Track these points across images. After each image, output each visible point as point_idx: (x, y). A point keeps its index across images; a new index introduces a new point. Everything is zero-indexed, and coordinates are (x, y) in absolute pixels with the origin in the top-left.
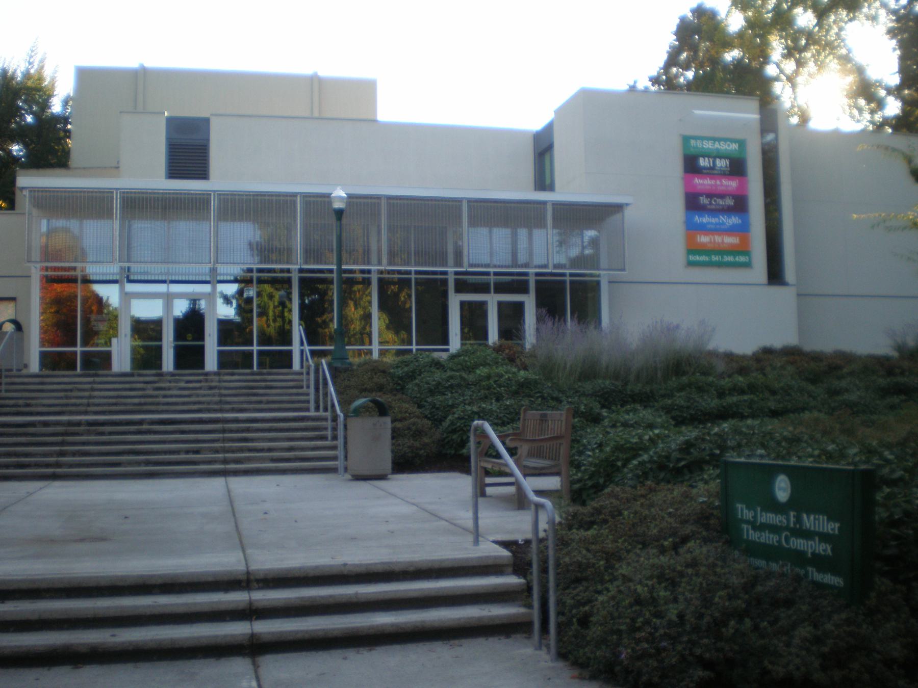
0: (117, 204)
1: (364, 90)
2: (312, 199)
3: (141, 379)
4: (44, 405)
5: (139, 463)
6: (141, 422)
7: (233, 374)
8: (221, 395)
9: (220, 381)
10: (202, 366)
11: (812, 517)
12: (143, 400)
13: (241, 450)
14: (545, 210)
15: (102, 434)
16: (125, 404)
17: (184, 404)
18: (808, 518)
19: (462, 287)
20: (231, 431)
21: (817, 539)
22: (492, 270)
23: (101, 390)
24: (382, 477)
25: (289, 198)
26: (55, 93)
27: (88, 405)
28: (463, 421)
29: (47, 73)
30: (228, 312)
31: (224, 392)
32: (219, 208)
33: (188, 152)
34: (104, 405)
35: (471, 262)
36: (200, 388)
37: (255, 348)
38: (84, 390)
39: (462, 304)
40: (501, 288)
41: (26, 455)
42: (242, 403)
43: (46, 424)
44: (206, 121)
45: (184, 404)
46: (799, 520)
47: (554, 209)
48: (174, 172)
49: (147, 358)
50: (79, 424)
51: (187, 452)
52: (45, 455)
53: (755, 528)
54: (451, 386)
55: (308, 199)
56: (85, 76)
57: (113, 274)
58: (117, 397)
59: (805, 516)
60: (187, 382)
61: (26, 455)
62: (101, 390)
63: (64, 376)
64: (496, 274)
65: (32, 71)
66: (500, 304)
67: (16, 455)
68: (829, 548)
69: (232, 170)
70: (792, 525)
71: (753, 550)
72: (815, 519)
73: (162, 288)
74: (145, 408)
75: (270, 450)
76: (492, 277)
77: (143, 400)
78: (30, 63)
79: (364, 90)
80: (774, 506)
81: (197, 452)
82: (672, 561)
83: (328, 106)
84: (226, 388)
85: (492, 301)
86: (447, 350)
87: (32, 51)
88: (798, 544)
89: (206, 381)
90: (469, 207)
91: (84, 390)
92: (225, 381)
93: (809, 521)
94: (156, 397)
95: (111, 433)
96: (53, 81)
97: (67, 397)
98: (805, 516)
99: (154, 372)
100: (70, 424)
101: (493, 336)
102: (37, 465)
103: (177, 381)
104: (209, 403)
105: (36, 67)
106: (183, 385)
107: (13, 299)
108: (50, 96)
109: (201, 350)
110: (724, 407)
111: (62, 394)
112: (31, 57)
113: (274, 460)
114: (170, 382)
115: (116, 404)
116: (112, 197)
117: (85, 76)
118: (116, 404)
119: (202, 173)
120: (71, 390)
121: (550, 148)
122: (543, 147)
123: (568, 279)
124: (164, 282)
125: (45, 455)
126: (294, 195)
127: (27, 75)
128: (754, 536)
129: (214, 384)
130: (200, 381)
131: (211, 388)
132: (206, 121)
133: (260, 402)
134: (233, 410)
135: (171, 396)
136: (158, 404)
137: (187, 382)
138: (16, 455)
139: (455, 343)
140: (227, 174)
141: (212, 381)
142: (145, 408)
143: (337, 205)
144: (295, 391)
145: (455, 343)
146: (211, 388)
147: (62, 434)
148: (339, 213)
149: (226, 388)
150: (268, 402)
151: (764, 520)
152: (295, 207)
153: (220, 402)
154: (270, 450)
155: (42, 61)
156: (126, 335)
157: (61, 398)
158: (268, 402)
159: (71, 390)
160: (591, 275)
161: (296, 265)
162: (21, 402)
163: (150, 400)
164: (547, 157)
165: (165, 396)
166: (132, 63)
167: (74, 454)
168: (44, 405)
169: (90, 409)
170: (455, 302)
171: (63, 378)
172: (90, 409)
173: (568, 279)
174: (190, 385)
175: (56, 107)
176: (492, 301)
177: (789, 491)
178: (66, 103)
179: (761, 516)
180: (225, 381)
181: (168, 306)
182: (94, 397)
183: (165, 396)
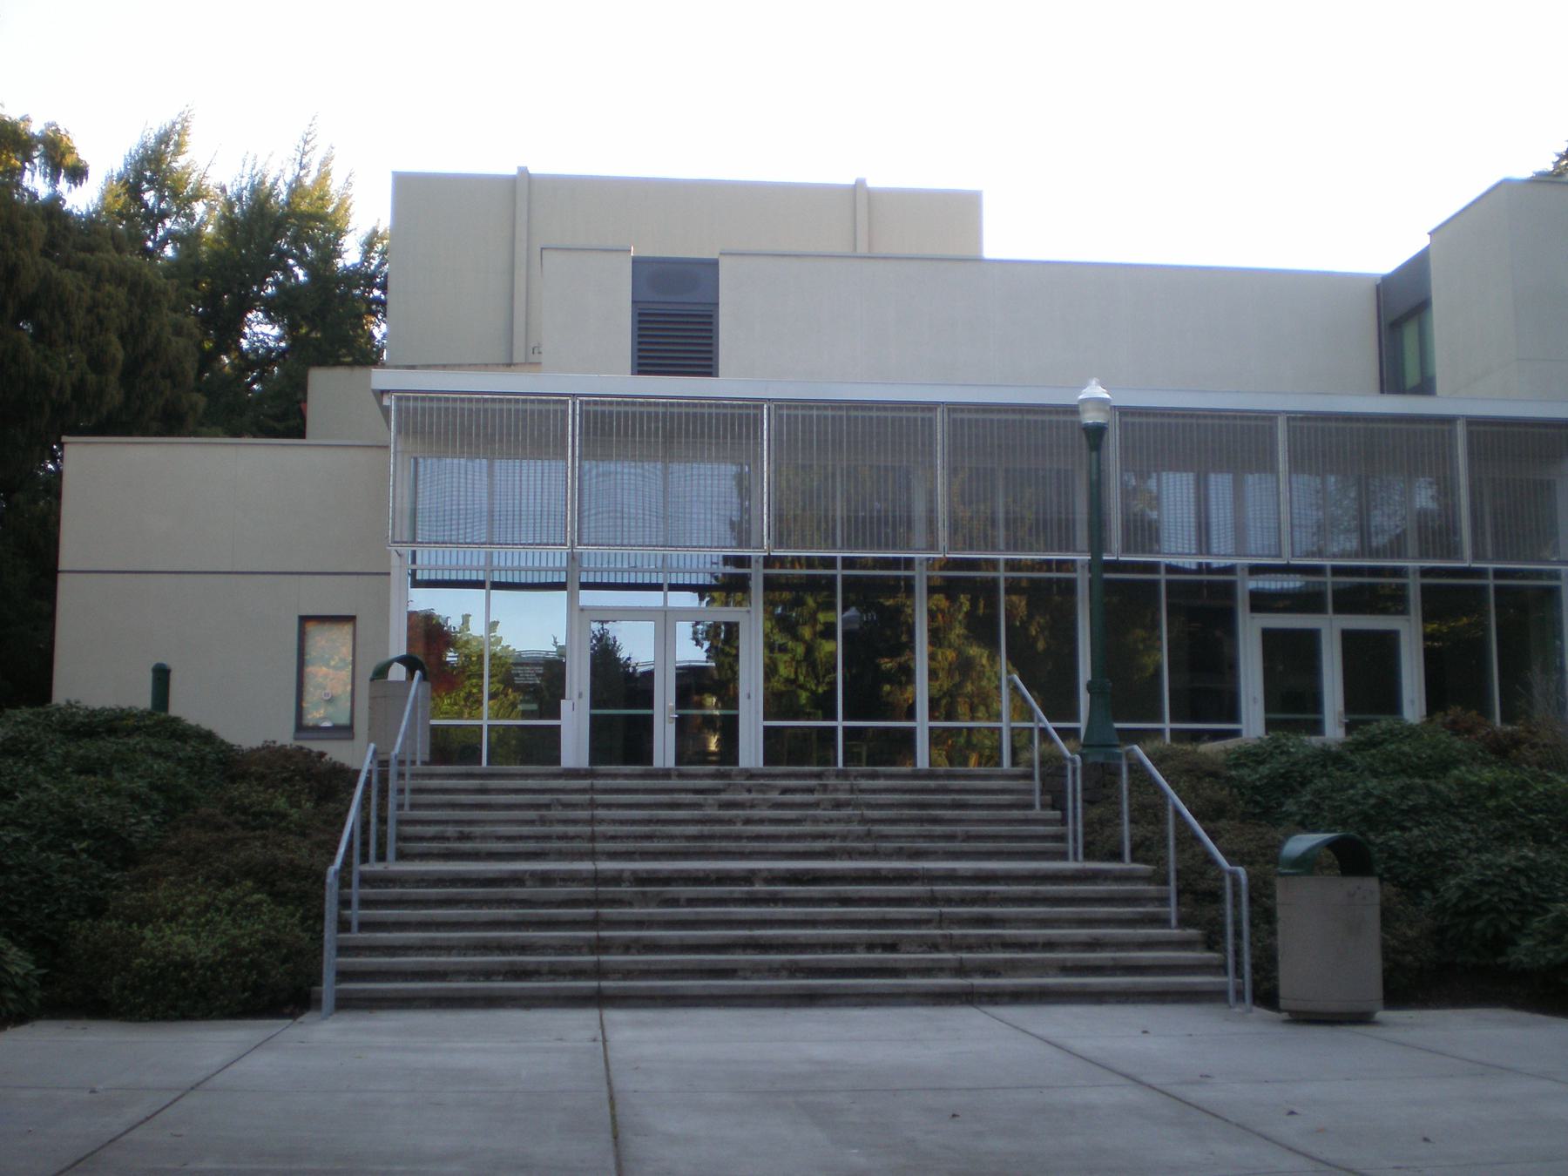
0: (573, 427)
1: (961, 209)
2: (966, 416)
3: (690, 783)
4: (499, 838)
5: (774, 971)
6: (748, 878)
7: (874, 776)
8: (863, 821)
9: (852, 791)
10: (648, 759)
12: (706, 829)
13: (987, 944)
14: (1452, 435)
15: (674, 902)
16: (671, 837)
17: (791, 837)
19: (1261, 602)
20: (949, 901)
22: (1328, 563)
23: (608, 806)
24: (1361, 1018)
25: (920, 415)
26: (351, 226)
27: (593, 838)
28: (1495, 889)
29: (335, 186)
30: (692, 653)
31: (869, 813)
32: (779, 433)
33: (676, 321)
34: (627, 837)
35: (347, 629)
36: (816, 805)
37: (840, 723)
38: (573, 806)
39: (1268, 635)
40: (1348, 602)
41: (523, 948)
42: (912, 837)
43: (545, 879)
44: (714, 264)
45: (791, 837)
47: (1470, 434)
48: (643, 365)
49: (622, 737)
50: (616, 879)
51: (871, 947)
52: (565, 948)
54: (1415, 810)
55: (959, 416)
56: (412, 191)
57: (554, 570)
58: (649, 822)
60: (785, 791)
61: (523, 948)
62: (608, 806)
63: (615, 776)
64: (1337, 571)
65: (308, 182)
66: (1348, 637)
67: (502, 948)
69: (757, 362)
73: (653, 599)
74: (716, 845)
75: (1050, 945)
76: (1329, 580)
77: (706, 829)
78: (302, 167)
79: (961, 209)
81: (892, 947)
83: (903, 240)
84: (870, 806)
85: (1330, 628)
86: (1235, 733)
87: (306, 142)
89: (825, 789)
90: (1291, 431)
91: (573, 806)
92: (862, 791)
94: (730, 822)
95: (691, 902)
96: (343, 206)
97: (543, 821)
99: (638, 768)
100: (597, 879)
101: (1413, 705)
102: (555, 972)
103: (763, 790)
104: (844, 838)
105: (314, 174)
106: (775, 796)
107: (351, 619)
108: (340, 233)
109: (645, 726)
111: (532, 814)
112: (304, 154)
113: (1066, 969)
114: (749, 791)
115: (649, 837)
116: (565, 413)
117: (412, 191)
118: (649, 837)
119: (706, 366)
120: (547, 806)
121: (1421, 308)
122: (1401, 310)
123: (1491, 582)
124: (657, 587)
125: (565, 948)
126: (931, 407)
127: (296, 188)
129: (843, 796)
130: (811, 790)
131: (838, 805)
132: (714, 264)
133: (951, 837)
134: (899, 854)
135: (761, 821)
136: (738, 838)
137: (785, 791)
138: (502, 948)
139: (1252, 722)
140: (751, 366)
141: (836, 790)
142: (716, 845)
143: (1091, 417)
144: (1016, 814)
145: (1252, 722)
146: (838, 805)
147: (588, 903)
148: (1096, 434)
149: (870, 806)
150: (969, 838)
152: (932, 435)
153: (868, 835)
154: (1050, 945)
155: (325, 163)
156: (580, 695)
157: (532, 822)
158: (969, 838)
159: (547, 806)
160: (1538, 574)
161: (924, 555)
162: (451, 830)
163: (717, 829)
164: (1410, 334)
165: (748, 821)
166: (494, 159)
167: (627, 947)
168: (499, 838)
169: (600, 846)
170: (1250, 633)
171: (449, 777)
172: (600, 846)
173: (1491, 582)
174: (788, 798)
175: (350, 255)
176: (1330, 628)
178: (369, 245)
180: (862, 791)
181: (665, 640)
182: (602, 821)
183: (748, 821)
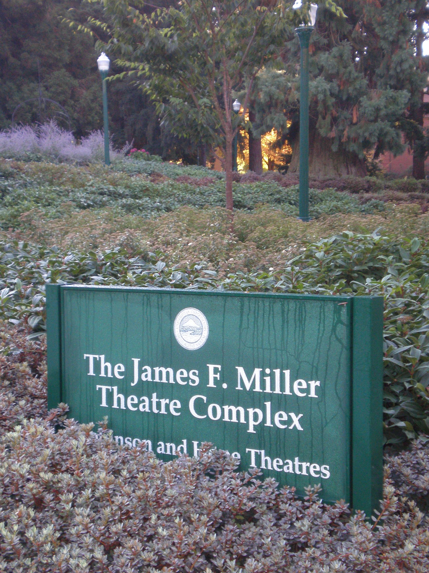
11: (257, 372)
18: (249, 374)
21: (268, 404)
46: (228, 375)
53: (126, 391)
59: (241, 371)
68: (296, 420)
70: (211, 384)
71: (123, 424)
72: (263, 374)
80: (174, 356)
82: (96, 476)
88: (232, 413)
93: (249, 379)
98: (241, 371)
110: (193, 125)
128: (124, 402)
151: (147, 377)
177: (206, 333)
179: (141, 372)
